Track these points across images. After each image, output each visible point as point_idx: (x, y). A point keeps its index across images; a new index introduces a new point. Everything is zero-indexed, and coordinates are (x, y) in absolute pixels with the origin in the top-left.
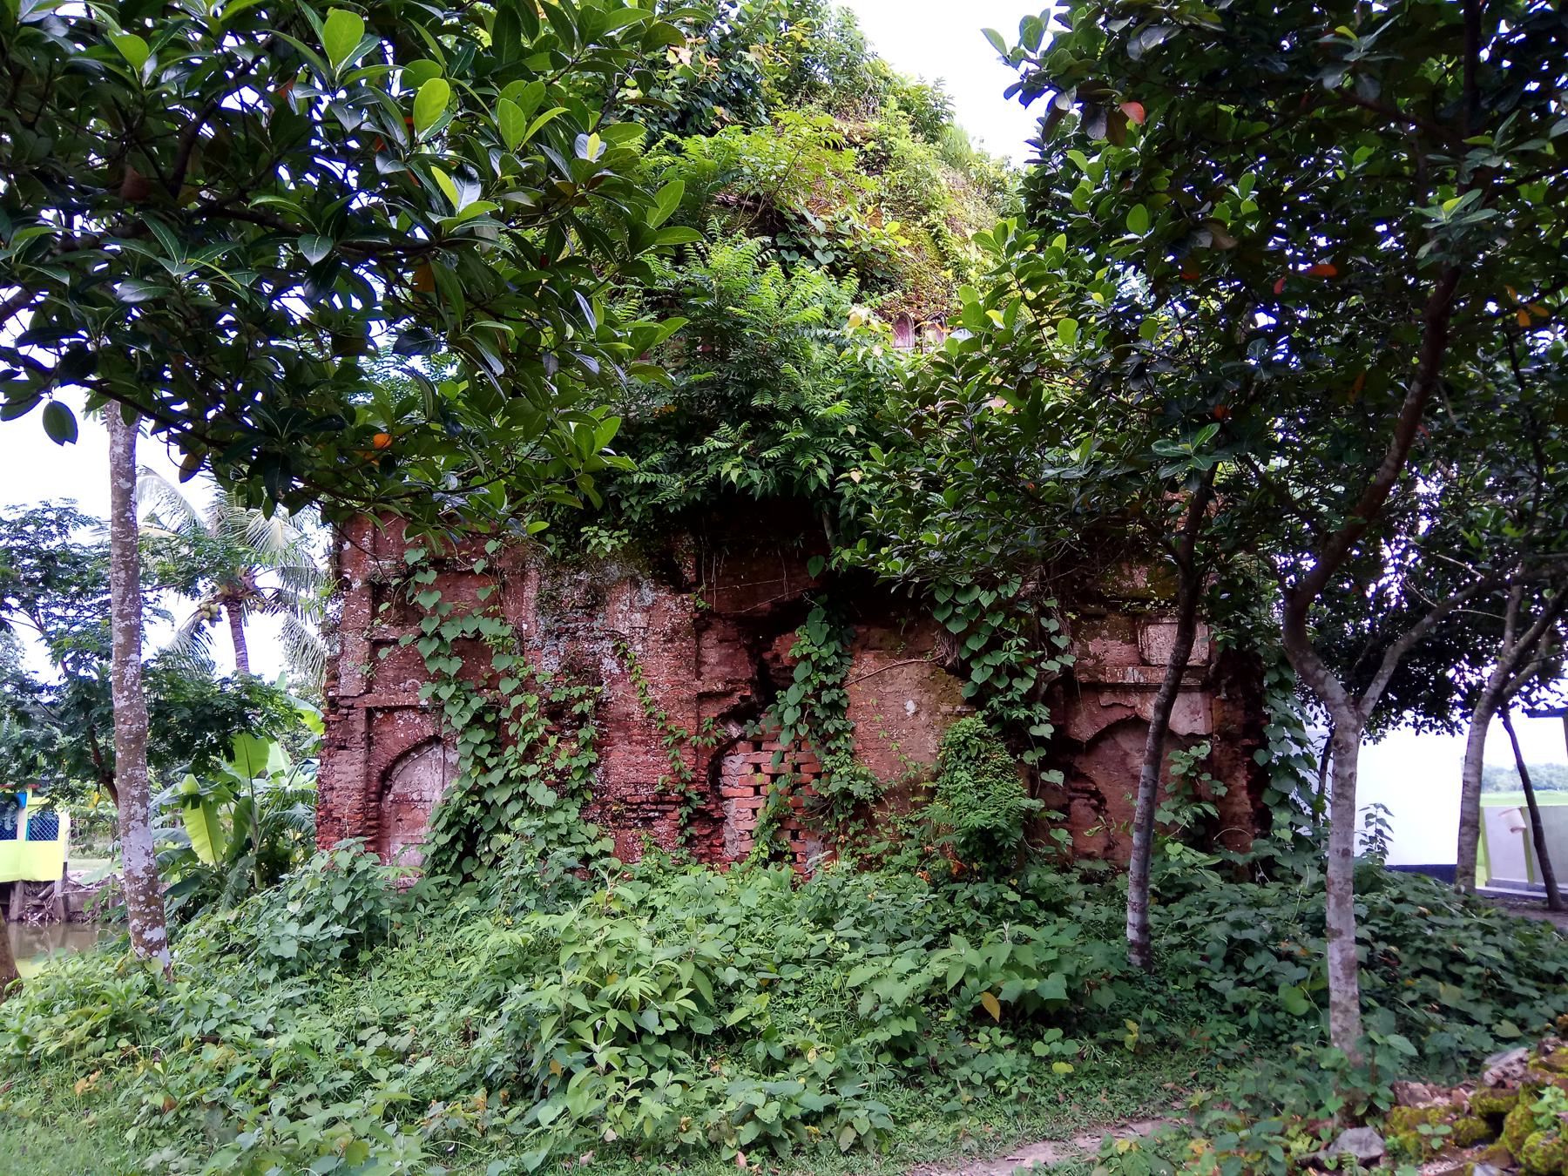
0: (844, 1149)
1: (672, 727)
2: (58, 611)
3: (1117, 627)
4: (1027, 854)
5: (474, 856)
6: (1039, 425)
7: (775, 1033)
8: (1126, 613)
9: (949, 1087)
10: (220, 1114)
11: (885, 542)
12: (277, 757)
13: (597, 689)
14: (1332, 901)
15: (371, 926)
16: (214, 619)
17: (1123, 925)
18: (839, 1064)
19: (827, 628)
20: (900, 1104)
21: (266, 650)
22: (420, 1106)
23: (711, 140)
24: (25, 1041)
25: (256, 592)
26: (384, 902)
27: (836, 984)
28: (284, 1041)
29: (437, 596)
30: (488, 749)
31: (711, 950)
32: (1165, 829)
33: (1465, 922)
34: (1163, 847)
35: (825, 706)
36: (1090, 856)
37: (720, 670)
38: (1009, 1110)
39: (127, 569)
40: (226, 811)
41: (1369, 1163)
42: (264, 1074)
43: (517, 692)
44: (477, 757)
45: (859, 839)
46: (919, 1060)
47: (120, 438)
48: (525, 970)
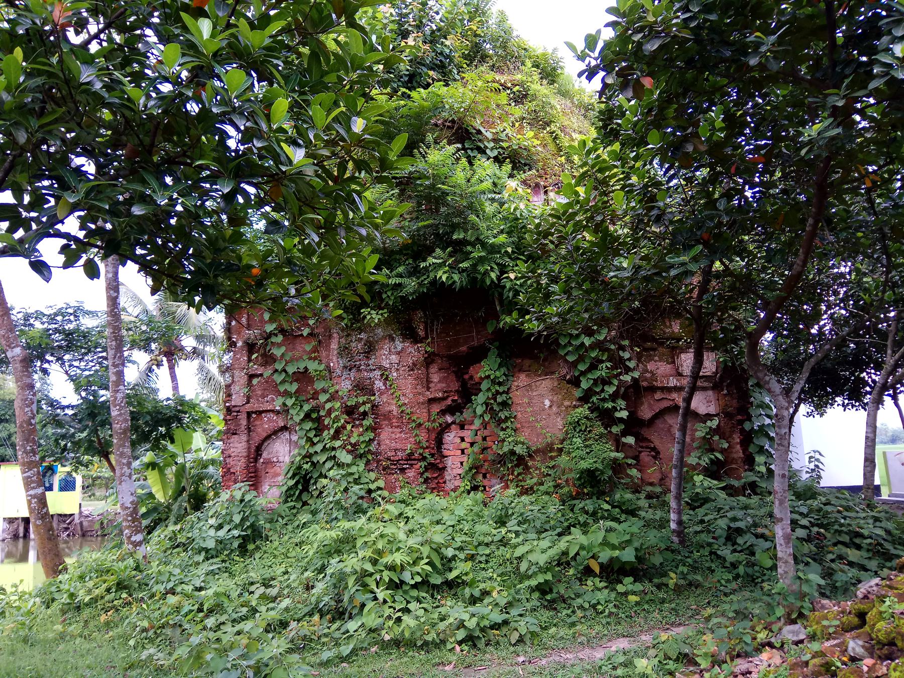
0: (513, 643)
1: (414, 418)
3: (664, 355)
5: (308, 492)
7: (475, 583)
9: (571, 610)
10: (179, 631)
11: (528, 312)
12: (198, 439)
13: (373, 398)
14: (777, 503)
15: (254, 531)
16: (159, 365)
17: (668, 521)
18: (510, 598)
19: (499, 360)
22: (284, 624)
23: (427, 91)
24: (72, 596)
25: (182, 349)
26: (260, 517)
27: (508, 556)
28: (210, 592)
29: (283, 349)
30: (314, 432)
31: (439, 539)
32: (694, 468)
34: (692, 477)
35: (499, 404)
37: (440, 386)
38: (604, 621)
39: (116, 340)
40: (171, 472)
41: (797, 643)
42: (200, 610)
43: (328, 401)
44: (308, 437)
45: (520, 478)
46: (554, 595)
48: (339, 552)
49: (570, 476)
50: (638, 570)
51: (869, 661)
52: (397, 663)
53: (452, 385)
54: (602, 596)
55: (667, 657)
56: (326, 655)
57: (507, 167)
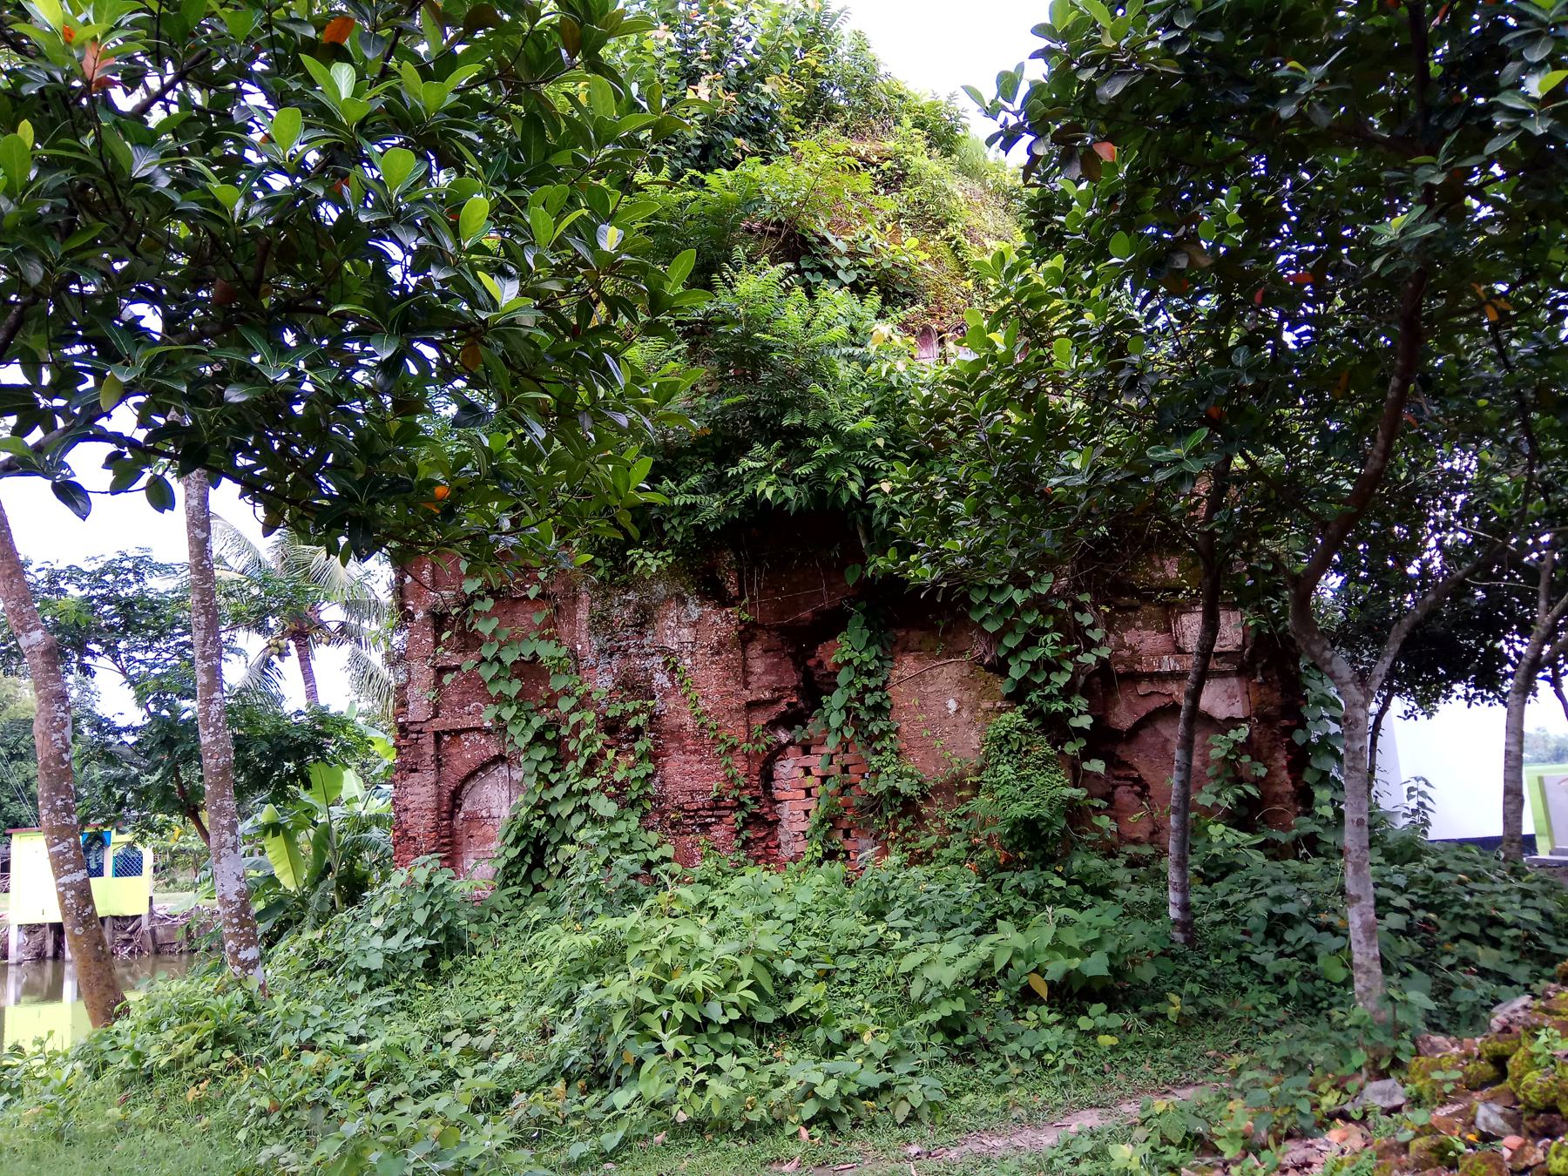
0: (900, 1120)
1: (723, 736)
2: (138, 655)
3: (1151, 617)
4: (1072, 841)
5: (543, 867)
6: (1051, 432)
8: (1159, 603)
9: (999, 1063)
10: (323, 1113)
11: (915, 550)
12: (351, 783)
13: (650, 703)
14: (1350, 868)
18: (893, 1045)
19: (867, 633)
20: (953, 1079)
21: (331, 682)
22: (504, 1098)
23: (732, 173)
24: (138, 1056)
25: (322, 626)
26: (461, 914)
27: (889, 972)
28: (376, 1045)
29: (495, 622)
30: (550, 765)
31: (769, 944)
32: (1208, 812)
33: (1505, 887)
34: (1205, 828)
35: (869, 709)
36: (1136, 842)
37: (766, 679)
38: (1057, 1081)
39: (206, 613)
40: (305, 838)
41: (1389, 1112)
42: (359, 1077)
43: (575, 709)
45: (908, 835)
46: (970, 1038)
47: (194, 491)
48: (596, 971)
49: (994, 830)
50: (1115, 991)
51: (1513, 1141)
52: (699, 1161)
53: (786, 678)
54: (1052, 1037)
55: (1165, 1141)
56: (577, 1150)
57: (874, 301)
